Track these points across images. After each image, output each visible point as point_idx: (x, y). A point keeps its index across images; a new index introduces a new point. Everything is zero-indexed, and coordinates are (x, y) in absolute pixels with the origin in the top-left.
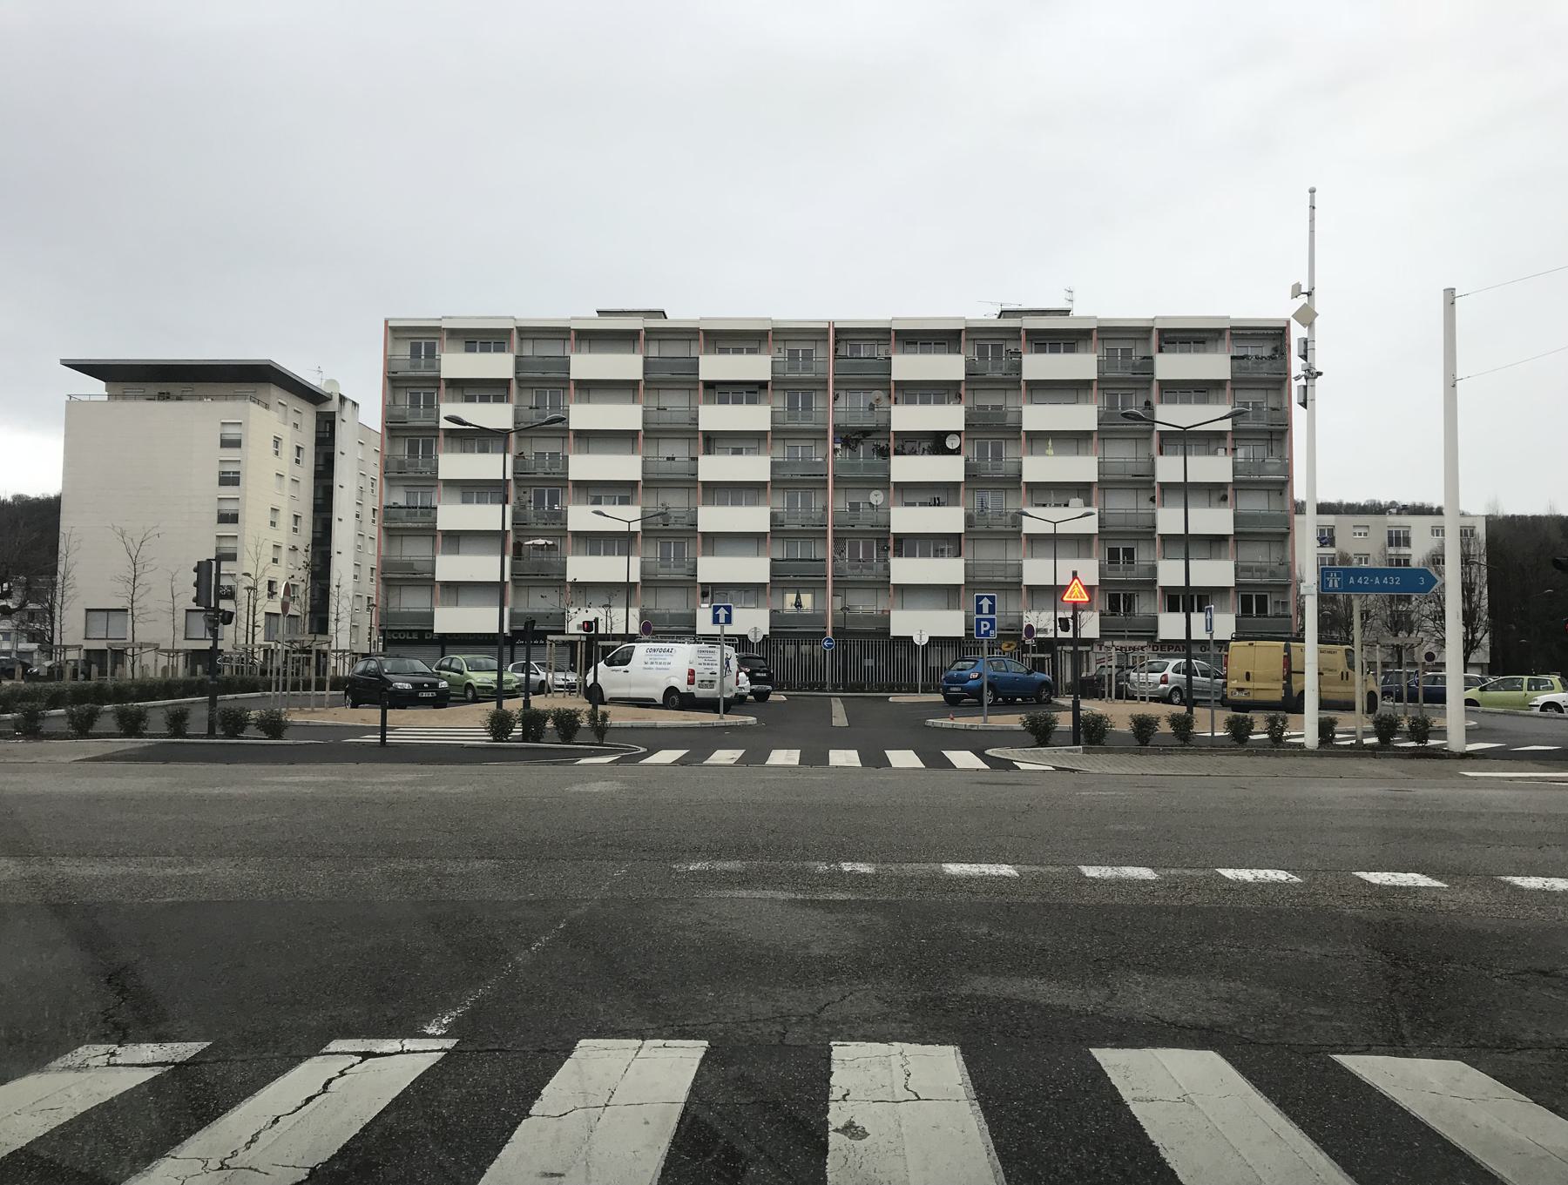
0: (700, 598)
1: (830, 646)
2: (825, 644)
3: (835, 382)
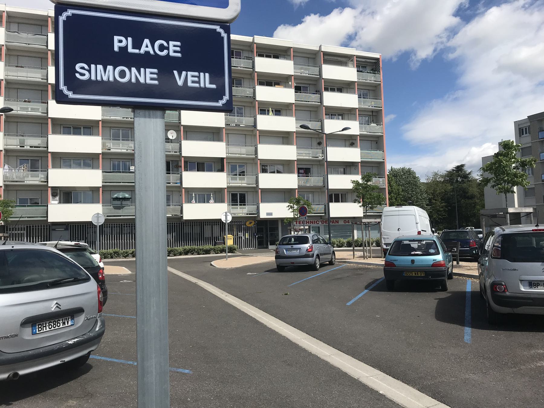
0: (50, 197)
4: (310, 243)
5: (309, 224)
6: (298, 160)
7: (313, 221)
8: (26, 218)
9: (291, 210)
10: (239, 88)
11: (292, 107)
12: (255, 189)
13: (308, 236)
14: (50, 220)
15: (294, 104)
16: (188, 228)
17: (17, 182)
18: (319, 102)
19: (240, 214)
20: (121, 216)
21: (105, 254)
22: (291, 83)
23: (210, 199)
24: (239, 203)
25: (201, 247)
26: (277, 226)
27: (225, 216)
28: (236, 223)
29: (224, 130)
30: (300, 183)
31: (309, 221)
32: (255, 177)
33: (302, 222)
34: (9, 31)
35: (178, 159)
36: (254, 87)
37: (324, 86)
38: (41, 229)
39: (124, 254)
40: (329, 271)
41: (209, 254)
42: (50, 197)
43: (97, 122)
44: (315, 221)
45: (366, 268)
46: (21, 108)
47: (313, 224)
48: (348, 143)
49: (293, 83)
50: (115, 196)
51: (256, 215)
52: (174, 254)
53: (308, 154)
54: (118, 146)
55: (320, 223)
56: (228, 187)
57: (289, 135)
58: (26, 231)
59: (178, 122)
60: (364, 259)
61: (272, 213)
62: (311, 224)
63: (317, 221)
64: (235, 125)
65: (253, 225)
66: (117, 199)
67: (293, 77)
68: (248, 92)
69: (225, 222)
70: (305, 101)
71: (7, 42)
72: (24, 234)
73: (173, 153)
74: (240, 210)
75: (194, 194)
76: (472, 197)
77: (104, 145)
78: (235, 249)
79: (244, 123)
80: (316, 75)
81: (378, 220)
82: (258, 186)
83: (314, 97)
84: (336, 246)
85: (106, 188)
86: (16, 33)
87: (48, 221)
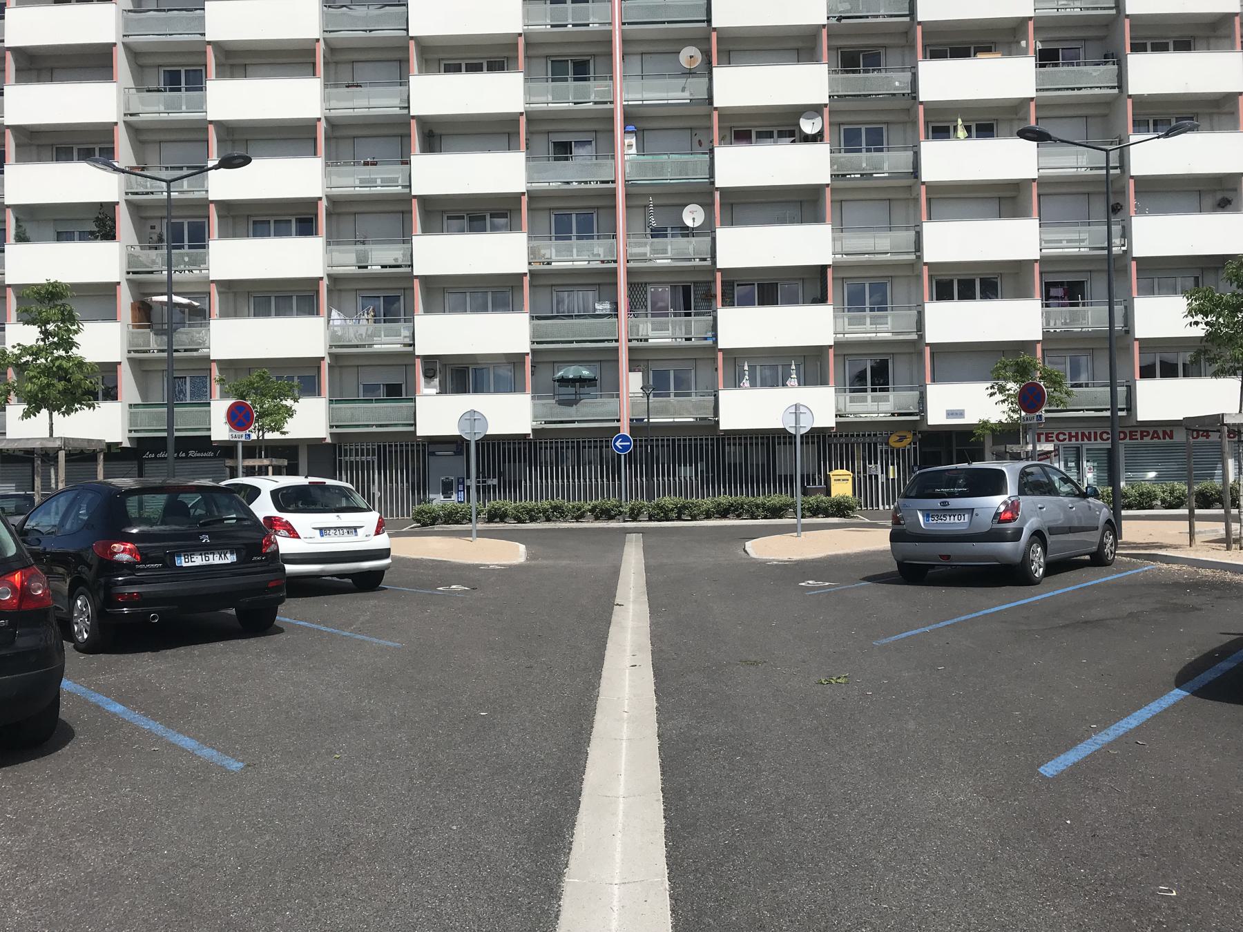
0: (421, 379)
1: (625, 448)
2: (618, 444)
3: (625, 42)
4: (1007, 494)
5: (1077, 440)
6: (1044, 261)
7: (1090, 433)
8: (374, 427)
9: (999, 397)
10: (870, 75)
11: (1028, 111)
12: (914, 347)
13: (1004, 469)
14: (421, 432)
15: (1032, 99)
16: (752, 450)
17: (357, 346)
18: (1113, 87)
19: (871, 415)
20: (573, 422)
21: (532, 510)
22: (1025, 42)
23: (789, 376)
24: (869, 386)
25: (760, 500)
26: (981, 448)
27: (794, 416)
28: (861, 440)
29: (828, 190)
30: (1052, 324)
31: (1077, 433)
32: (916, 312)
33: (1054, 436)
34: (329, 7)
35: (710, 279)
36: (914, 67)
37: (1131, 38)
38: (407, 451)
39: (574, 513)
40: (1078, 587)
41: (780, 518)
42: (421, 379)
43: (517, 197)
44: (1095, 433)
45: (1229, 584)
46: (361, 181)
47: (1089, 439)
48: (1208, 201)
49: (1032, 43)
50: (560, 374)
51: (917, 418)
52: (691, 517)
53: (1075, 241)
54: (569, 253)
56: (838, 345)
57: (1019, 192)
58: (376, 457)
59: (707, 180)
60: (1228, 548)
61: (964, 410)
62: (1083, 440)
64: (859, 176)
65: (910, 444)
66: (563, 381)
67: (1031, 24)
68: (897, 84)
69: (794, 433)
70: (1067, 89)
71: (327, 31)
72: (373, 462)
73: (697, 262)
74: (873, 403)
75: (746, 364)
77: (532, 252)
78: (852, 508)
79: (886, 168)
80: (1105, 8)
82: (921, 337)
83: (1098, 73)
84: (1159, 503)
85: (542, 357)
86: (344, 8)
87: (418, 435)
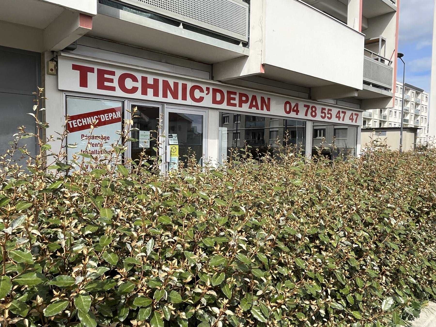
5: (156, 94)
31: (156, 81)
33: (116, 79)
44: (184, 87)
47: (175, 96)
55: (208, 102)
62: (165, 96)
63: (193, 88)
76: (46, 254)
81: (260, 108)
